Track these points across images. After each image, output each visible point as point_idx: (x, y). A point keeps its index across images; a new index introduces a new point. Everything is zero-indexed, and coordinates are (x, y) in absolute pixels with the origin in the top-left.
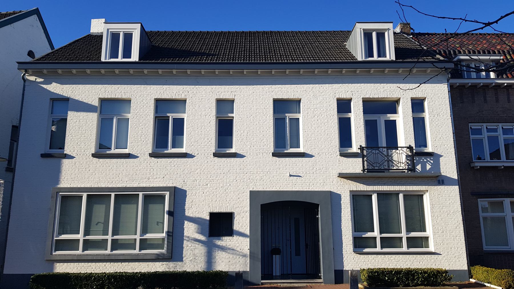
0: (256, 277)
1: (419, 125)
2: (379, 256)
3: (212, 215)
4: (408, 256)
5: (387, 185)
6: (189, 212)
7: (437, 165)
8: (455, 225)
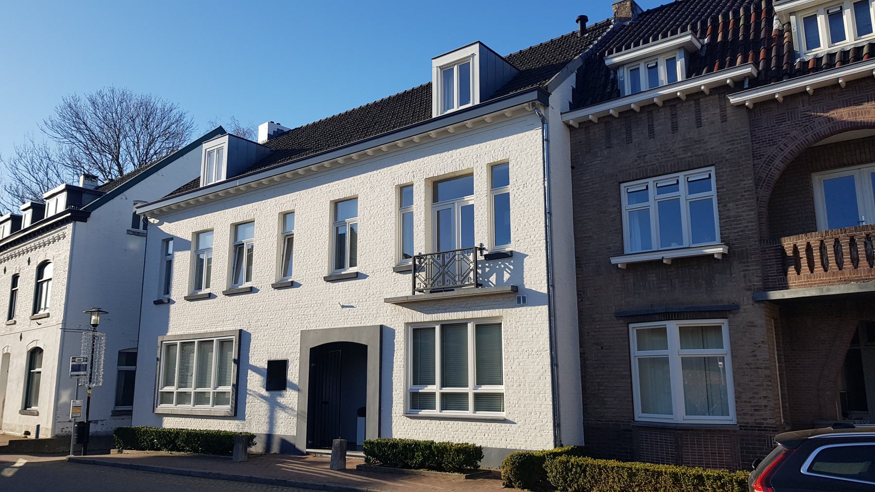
0: (302, 445)
1: (501, 207)
2: (434, 421)
3: (270, 363)
4: (469, 423)
5: (449, 312)
6: (252, 361)
7: (519, 271)
8: (539, 374)
